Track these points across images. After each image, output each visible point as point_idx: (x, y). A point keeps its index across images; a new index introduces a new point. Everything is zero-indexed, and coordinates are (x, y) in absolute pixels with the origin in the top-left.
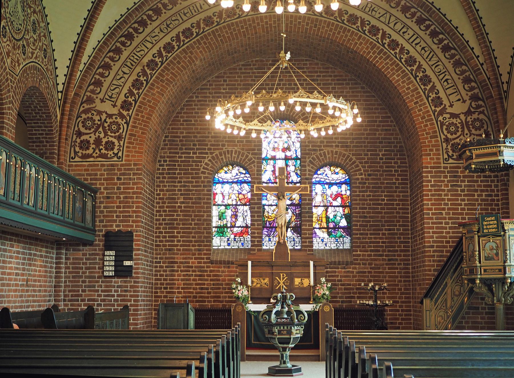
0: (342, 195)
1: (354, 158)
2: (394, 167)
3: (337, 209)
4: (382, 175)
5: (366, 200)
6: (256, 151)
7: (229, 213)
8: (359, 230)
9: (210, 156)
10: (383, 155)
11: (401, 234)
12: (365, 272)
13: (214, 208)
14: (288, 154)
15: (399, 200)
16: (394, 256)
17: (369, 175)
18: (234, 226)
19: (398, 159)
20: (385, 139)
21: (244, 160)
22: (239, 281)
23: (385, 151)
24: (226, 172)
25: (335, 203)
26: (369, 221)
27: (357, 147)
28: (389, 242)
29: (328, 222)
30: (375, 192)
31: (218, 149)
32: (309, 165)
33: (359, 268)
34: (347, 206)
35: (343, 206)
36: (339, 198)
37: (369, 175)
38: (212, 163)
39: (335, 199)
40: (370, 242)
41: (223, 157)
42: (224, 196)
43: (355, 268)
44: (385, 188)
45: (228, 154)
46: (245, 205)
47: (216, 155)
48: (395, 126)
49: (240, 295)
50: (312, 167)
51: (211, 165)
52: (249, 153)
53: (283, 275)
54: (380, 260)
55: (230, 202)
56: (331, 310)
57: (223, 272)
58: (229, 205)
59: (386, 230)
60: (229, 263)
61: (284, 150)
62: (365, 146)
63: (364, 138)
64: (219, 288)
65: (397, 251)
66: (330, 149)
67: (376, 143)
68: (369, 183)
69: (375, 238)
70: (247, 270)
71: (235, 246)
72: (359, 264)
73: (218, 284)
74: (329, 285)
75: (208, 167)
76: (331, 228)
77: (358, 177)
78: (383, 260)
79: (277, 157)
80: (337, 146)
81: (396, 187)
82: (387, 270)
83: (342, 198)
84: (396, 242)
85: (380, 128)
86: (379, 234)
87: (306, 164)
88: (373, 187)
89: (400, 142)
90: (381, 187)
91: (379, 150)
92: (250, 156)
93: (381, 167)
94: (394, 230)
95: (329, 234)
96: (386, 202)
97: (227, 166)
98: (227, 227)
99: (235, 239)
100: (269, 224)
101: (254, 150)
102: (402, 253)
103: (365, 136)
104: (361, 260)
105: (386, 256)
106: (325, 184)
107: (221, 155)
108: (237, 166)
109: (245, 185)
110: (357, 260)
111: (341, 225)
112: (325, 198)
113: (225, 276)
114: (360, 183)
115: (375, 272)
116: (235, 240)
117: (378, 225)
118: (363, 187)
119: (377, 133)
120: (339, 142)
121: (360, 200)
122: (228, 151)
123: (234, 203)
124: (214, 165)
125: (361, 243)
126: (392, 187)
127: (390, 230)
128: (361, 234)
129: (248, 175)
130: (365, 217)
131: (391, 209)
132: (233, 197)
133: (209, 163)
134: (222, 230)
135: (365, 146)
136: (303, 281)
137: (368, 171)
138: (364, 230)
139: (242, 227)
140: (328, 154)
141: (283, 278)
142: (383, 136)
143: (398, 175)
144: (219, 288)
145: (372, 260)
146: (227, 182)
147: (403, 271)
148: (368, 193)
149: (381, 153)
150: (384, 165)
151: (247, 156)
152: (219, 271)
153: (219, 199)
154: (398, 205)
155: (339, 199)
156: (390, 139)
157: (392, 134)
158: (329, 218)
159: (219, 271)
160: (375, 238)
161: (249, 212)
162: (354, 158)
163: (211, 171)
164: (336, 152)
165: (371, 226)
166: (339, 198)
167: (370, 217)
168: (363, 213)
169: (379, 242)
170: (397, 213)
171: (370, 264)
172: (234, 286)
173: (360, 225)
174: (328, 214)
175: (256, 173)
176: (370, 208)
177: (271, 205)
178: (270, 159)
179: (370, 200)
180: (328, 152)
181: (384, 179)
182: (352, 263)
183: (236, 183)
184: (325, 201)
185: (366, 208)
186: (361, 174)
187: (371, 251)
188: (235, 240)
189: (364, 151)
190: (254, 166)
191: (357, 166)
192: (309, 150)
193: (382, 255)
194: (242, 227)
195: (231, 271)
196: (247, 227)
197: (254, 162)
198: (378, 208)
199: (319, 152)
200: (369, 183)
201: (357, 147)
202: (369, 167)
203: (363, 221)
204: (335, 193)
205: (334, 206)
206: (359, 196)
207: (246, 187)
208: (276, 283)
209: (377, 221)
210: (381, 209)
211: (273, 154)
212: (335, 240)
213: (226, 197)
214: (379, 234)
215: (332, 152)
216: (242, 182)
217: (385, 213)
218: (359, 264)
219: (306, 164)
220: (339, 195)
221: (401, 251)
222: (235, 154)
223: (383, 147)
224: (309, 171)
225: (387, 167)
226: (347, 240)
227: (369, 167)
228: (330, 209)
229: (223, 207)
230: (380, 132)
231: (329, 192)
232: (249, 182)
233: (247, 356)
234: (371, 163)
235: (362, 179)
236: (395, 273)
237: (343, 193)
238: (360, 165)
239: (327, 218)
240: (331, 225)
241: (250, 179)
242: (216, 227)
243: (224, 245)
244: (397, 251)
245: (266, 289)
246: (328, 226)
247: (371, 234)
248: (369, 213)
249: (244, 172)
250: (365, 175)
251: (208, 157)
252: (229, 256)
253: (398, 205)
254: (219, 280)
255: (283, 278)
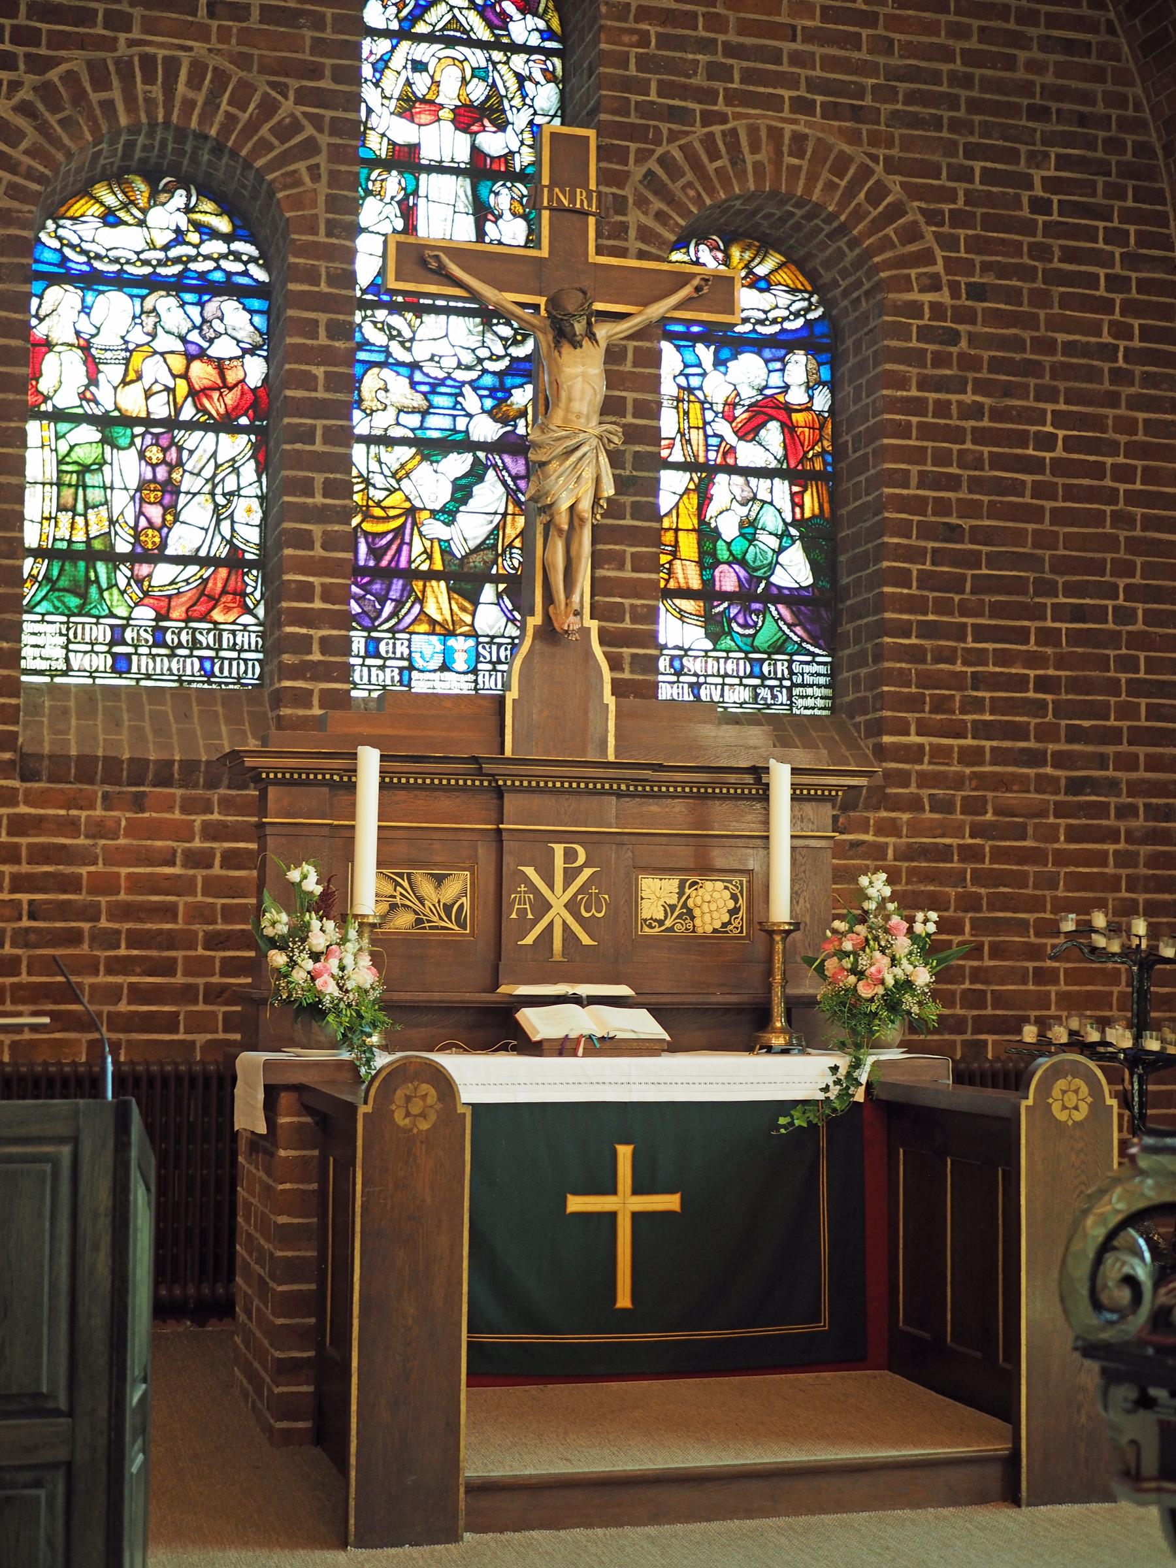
0: (789, 409)
1: (896, 193)
2: (1104, 260)
3: (762, 487)
4: (1040, 299)
5: (957, 435)
6: (325, 84)
7: (127, 468)
8: (915, 605)
9: (30, 79)
10: (1051, 184)
11: (1139, 641)
12: (944, 853)
13: (34, 430)
14: (493, 143)
15: (1133, 450)
16: (1101, 761)
17: (978, 292)
18: (159, 556)
19: (1128, 216)
20: (1058, 93)
21: (252, 127)
22: (312, 886)
23: (1064, 162)
24: (110, 219)
25: (748, 455)
26: (972, 560)
27: (916, 122)
28: (1075, 685)
29: (707, 560)
30: (1008, 391)
31: (82, 43)
32: (642, 202)
33: (916, 828)
34: (814, 476)
35: (792, 471)
36: (774, 426)
37: (978, 292)
38: (43, 129)
39: (749, 432)
40: (978, 681)
41: (116, 94)
42: (93, 366)
43: (890, 828)
44: (1060, 371)
45: (149, 79)
46: (225, 425)
47: (70, 78)
48: (1111, 30)
49: (330, 988)
50: (660, 216)
51: (32, 136)
52: (282, 89)
53: (570, 856)
54: (1023, 783)
55: (132, 402)
56: (1098, 1108)
57: (99, 830)
58: (128, 421)
59: (1059, 613)
60: (139, 771)
61: (468, 117)
62: (956, 126)
63: (954, 78)
64: (74, 938)
65: (1113, 736)
66: (764, 119)
67: (1012, 110)
68: (972, 337)
69: (1003, 658)
70: (351, 811)
71: (155, 669)
72: (914, 804)
73: (64, 910)
74: (927, 923)
75: (16, 154)
76: (724, 596)
77: (915, 296)
78: (1045, 784)
79: (428, 154)
80: (802, 106)
81: (1118, 376)
82: (1062, 845)
83: (788, 429)
84: (1113, 687)
85: (1033, 32)
86: (1022, 635)
87: (628, 192)
88: (996, 365)
89: (1139, 125)
90: (1034, 369)
91: (1032, 155)
92: (288, 106)
93: (1041, 252)
94: (1100, 614)
95: (716, 628)
96: (1059, 452)
97: (117, 178)
98: (113, 559)
99: (159, 634)
100: (374, 552)
101: (315, 72)
102: (1141, 751)
103: (958, 66)
104: (925, 780)
105: (1060, 760)
106: (695, 338)
107: (101, 83)
108: (183, 183)
109: (230, 307)
110: (902, 779)
111: (780, 578)
112: (695, 419)
113: (115, 857)
114: (925, 334)
115: (999, 855)
116: (159, 643)
117: (1018, 586)
118: (940, 360)
119: (1022, 55)
120: (813, 85)
121: (926, 431)
122: (148, 63)
123: (160, 408)
124: (55, 141)
125: (927, 681)
126: (1093, 374)
127: (1079, 614)
128: (928, 630)
129: (246, 248)
130: (953, 533)
131: (1091, 494)
132: (155, 371)
133: (21, 122)
134: (77, 568)
135: (956, 126)
136: (696, 898)
137: (966, 267)
138: (942, 607)
139: (204, 562)
140: (755, 148)
141: (570, 875)
142: (1049, 79)
143: (1130, 308)
144: (74, 938)
145: (982, 781)
146: (120, 281)
147: (1145, 850)
148: (969, 398)
149: (1037, 175)
150: (1057, 244)
151: (268, 108)
152: (70, 826)
153: (61, 378)
154: (1124, 474)
155: (773, 434)
156: (1086, 98)
157: (1098, 75)
158: (716, 535)
159: (70, 826)
160: (1003, 658)
161: (249, 471)
162: (894, 182)
163: (30, 175)
164: (799, 139)
165: (983, 585)
166: (774, 426)
167: (978, 535)
168: (942, 507)
169: (1020, 683)
170: (1120, 519)
171: (973, 806)
172: (277, 922)
173: (926, 580)
174: (712, 511)
175: (324, 216)
176: (976, 485)
177: (387, 441)
178: (387, 165)
179: (981, 436)
180: (753, 131)
181: (1054, 324)
182: (878, 798)
183: (175, 286)
184: (696, 437)
185: (953, 483)
186: (934, 284)
187: (983, 730)
188: (159, 643)
189: (949, 148)
190: (314, 171)
191: (912, 234)
192: (645, 110)
193: (1035, 758)
194: (204, 562)
195: (154, 830)
196: (234, 561)
197: (310, 147)
198: (1016, 488)
199: (700, 131)
200: (972, 337)
201: (916, 122)
202: (976, 245)
203: (938, 557)
204: (748, 394)
205: (748, 472)
206: (916, 407)
207: (237, 320)
208: (518, 904)
209: (1017, 561)
210: (1040, 490)
211: (403, 132)
212: (744, 668)
213: (112, 373)
214: (1022, 635)
215: (775, 134)
216: (207, 288)
217: (1059, 516)
218: (914, 804)
219: (628, 192)
220: (768, 408)
221: (1137, 736)
222: (195, 82)
223: (1049, 139)
224: (645, 234)
225: (1070, 255)
226: (813, 669)
227: (976, 245)
228: (724, 487)
229: (88, 433)
230: (1036, 54)
231: (716, 388)
232: (258, 290)
233: (483, 1488)
234: (989, 223)
235: (937, 310)
236: (1100, 859)
237: (797, 396)
238: (929, 230)
239: (707, 534)
240: (727, 579)
241: (261, 275)
242: (39, 553)
243: (91, 665)
244: (1113, 736)
245: (451, 945)
246: (708, 583)
247: (981, 633)
248: (970, 509)
249: (223, 225)
250: (955, 294)
251: (15, 86)
252: (137, 732)
253: (1124, 474)
254: (71, 884)
255: (570, 875)
